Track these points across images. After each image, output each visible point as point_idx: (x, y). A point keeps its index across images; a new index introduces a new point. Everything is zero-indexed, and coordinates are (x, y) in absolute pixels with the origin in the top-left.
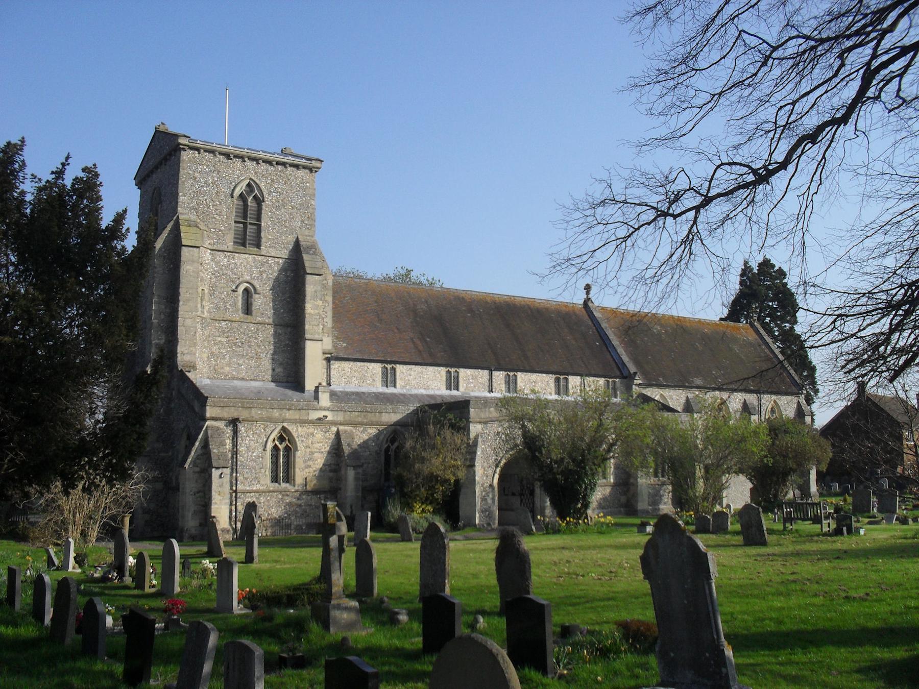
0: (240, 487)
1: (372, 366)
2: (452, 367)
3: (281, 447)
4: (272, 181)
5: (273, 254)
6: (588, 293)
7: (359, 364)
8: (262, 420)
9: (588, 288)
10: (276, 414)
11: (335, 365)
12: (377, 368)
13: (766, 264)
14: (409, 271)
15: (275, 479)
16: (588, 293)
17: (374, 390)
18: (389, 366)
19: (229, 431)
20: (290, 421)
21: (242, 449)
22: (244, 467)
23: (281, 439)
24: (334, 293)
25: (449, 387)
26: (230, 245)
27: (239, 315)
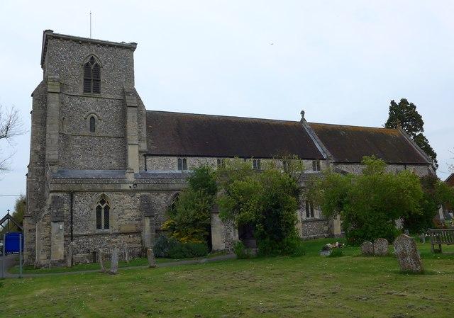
0: (74, 233)
1: (172, 158)
2: (221, 157)
3: (103, 207)
4: (107, 56)
5: (109, 97)
6: (303, 116)
7: (164, 158)
8: (89, 191)
9: (303, 113)
10: (99, 187)
11: (149, 159)
12: (175, 160)
13: (404, 102)
14: (393, 102)
15: (99, 226)
16: (303, 116)
17: (173, 172)
18: (182, 158)
19: (67, 199)
20: (108, 191)
21: (76, 209)
22: (78, 220)
23: (103, 202)
24: (147, 118)
25: (180, 168)
26: (80, 90)
27: (88, 133)
